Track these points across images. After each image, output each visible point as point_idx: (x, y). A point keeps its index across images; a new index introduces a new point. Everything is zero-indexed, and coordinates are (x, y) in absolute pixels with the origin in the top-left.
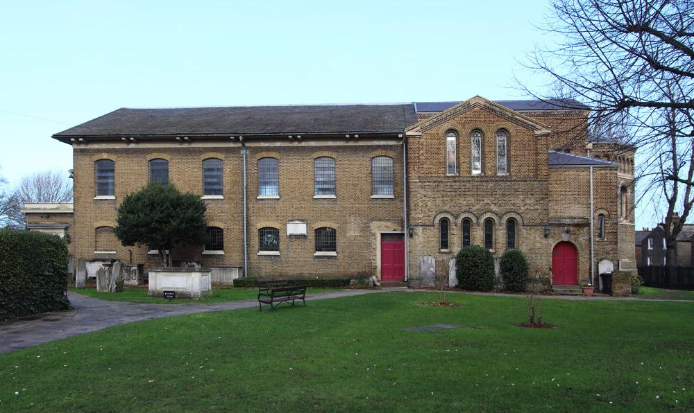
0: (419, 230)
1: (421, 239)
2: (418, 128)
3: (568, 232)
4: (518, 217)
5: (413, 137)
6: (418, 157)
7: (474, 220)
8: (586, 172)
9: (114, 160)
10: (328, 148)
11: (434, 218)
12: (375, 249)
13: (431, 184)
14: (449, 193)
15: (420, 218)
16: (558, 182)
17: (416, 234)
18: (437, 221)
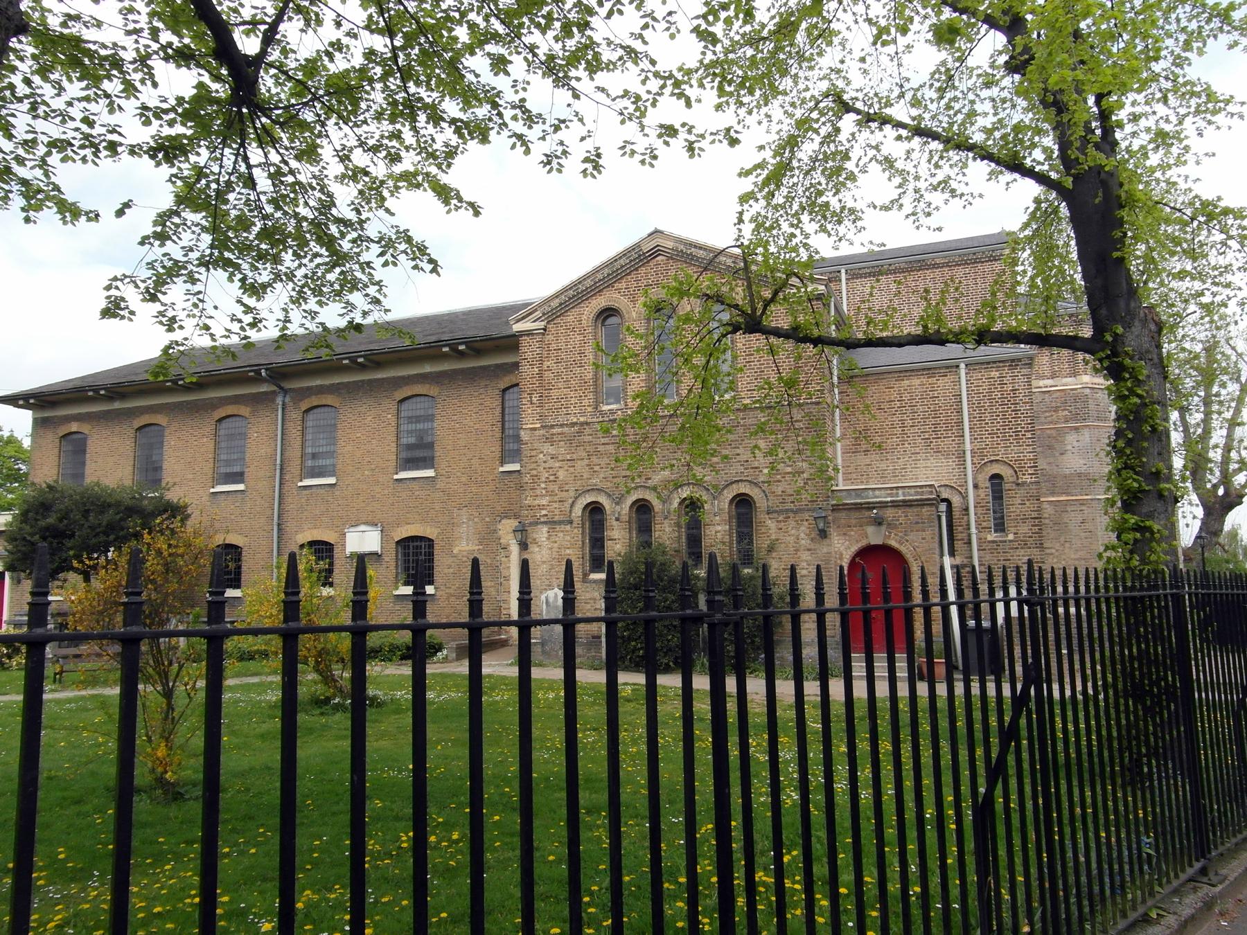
0: (542, 533)
1: (545, 552)
2: (538, 314)
3: (878, 522)
4: (754, 493)
5: (529, 333)
6: (540, 375)
7: (657, 504)
8: (951, 377)
9: (86, 432)
10: (423, 378)
11: (572, 505)
12: (507, 578)
13: (566, 429)
14: (601, 448)
15: (541, 507)
16: (885, 406)
17: (535, 541)
18: (578, 511)
